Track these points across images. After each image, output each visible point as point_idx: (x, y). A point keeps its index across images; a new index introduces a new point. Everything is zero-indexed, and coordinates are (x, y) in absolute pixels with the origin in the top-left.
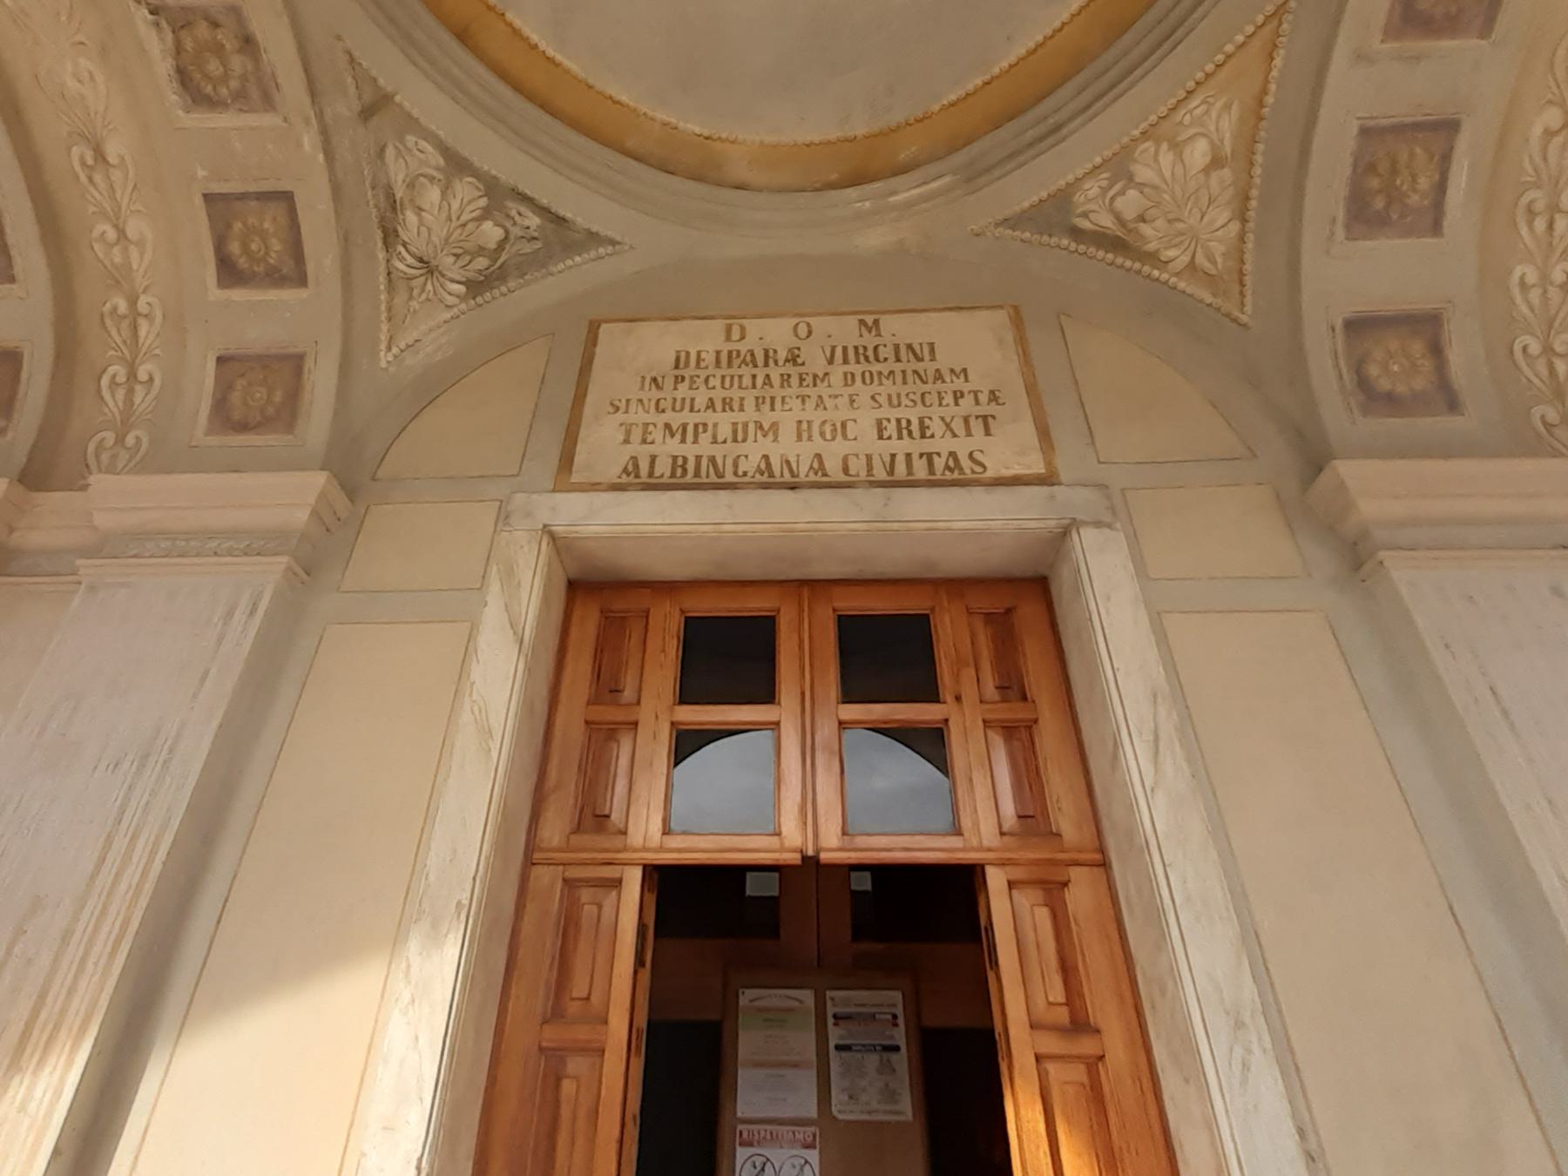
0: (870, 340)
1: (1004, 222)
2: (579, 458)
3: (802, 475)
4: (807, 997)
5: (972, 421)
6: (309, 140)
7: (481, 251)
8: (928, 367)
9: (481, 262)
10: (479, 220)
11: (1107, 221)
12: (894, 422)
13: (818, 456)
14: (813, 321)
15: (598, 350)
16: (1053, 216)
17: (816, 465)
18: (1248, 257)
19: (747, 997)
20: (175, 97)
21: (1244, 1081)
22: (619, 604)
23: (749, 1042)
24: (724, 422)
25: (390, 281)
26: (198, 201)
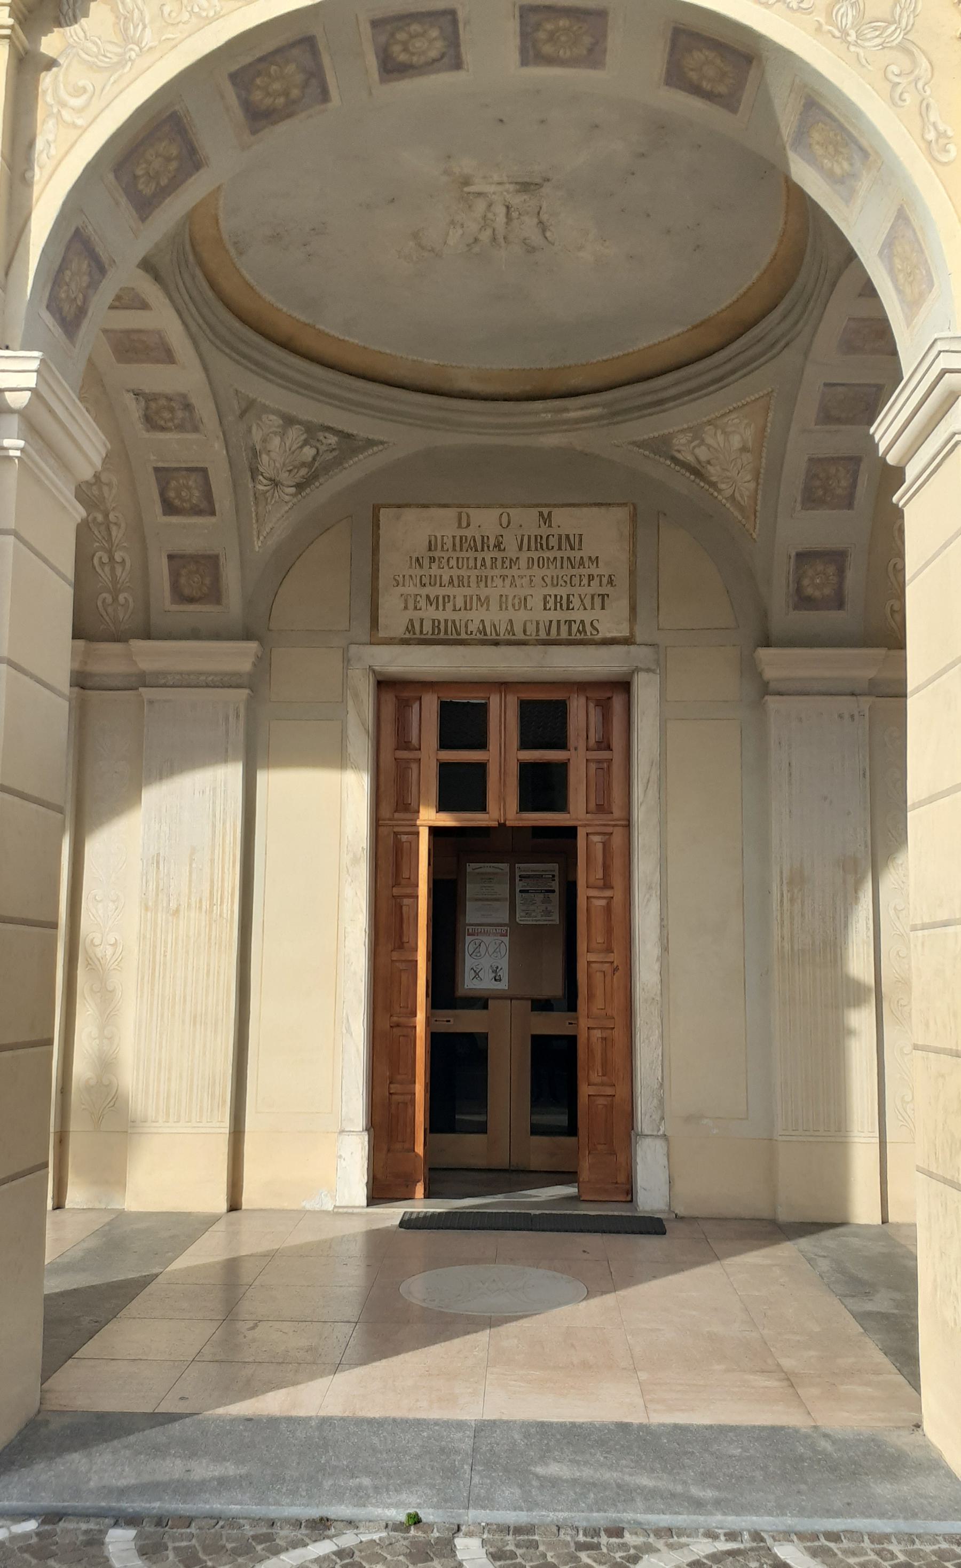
0: (544, 531)
1: (634, 443)
2: (381, 620)
3: (502, 634)
4: (505, 867)
5: (596, 597)
6: (218, 446)
7: (303, 464)
8: (577, 554)
9: (303, 471)
10: (301, 447)
11: (690, 458)
12: (553, 597)
13: (511, 621)
14: (512, 511)
15: (381, 532)
16: (660, 447)
17: (509, 628)
18: (759, 502)
19: (471, 867)
20: (141, 426)
21: (647, 905)
22: (406, 694)
23: (471, 889)
24: (459, 593)
25: (256, 498)
26: (151, 470)
